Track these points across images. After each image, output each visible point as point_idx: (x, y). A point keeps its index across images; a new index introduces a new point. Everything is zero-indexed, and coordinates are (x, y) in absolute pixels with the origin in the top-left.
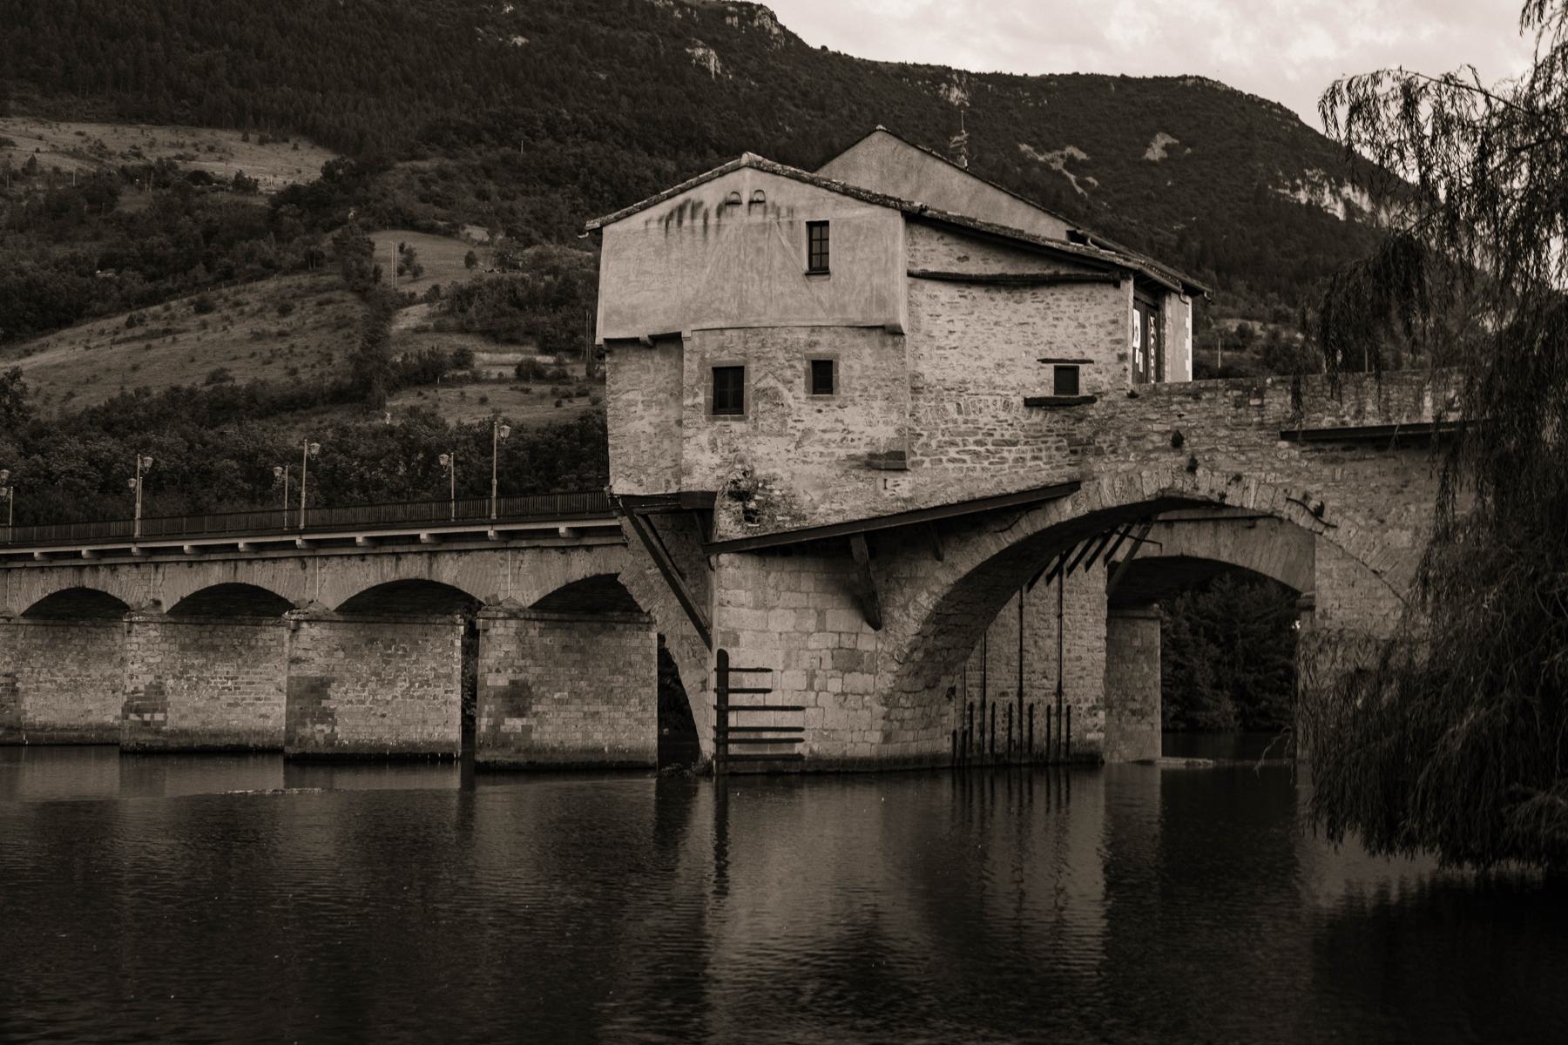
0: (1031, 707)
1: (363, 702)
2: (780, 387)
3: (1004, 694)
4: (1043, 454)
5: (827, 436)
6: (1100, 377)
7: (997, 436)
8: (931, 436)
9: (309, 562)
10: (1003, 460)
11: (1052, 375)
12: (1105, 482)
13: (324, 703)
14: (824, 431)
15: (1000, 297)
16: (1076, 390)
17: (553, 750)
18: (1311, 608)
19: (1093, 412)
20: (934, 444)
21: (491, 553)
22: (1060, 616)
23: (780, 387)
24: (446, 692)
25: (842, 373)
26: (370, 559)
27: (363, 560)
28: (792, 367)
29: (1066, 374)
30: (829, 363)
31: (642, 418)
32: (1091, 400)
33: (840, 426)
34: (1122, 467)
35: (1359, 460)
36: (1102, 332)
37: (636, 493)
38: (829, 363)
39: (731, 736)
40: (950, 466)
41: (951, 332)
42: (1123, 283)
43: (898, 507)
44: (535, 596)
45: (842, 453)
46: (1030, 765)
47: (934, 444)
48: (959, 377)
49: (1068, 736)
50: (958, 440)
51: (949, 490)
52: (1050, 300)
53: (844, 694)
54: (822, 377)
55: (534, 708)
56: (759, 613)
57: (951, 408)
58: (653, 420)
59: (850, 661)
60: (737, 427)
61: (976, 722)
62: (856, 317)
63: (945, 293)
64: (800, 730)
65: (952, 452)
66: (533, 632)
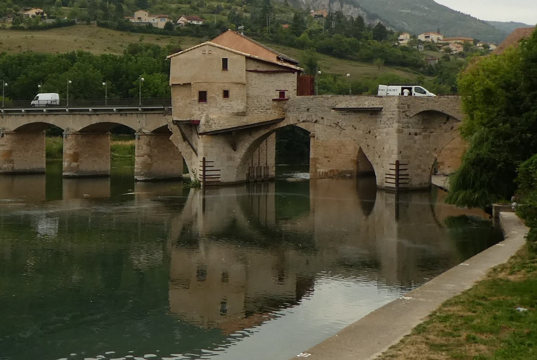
0: (261, 167)
1: (21, 157)
2: (216, 96)
3: (256, 164)
4: (277, 111)
5: (227, 108)
6: (289, 94)
7: (266, 108)
8: (251, 108)
9: (4, 116)
10: (267, 113)
11: (279, 93)
12: (291, 118)
13: (11, 158)
14: (226, 107)
15: (267, 76)
16: (284, 97)
17: (85, 171)
18: (314, 137)
19: (288, 102)
20: (252, 109)
21: (66, 115)
22: (266, 144)
23: (216, 96)
24: (42, 153)
25: (230, 94)
26: (25, 116)
27: (23, 116)
28: (219, 91)
29: (282, 94)
30: (228, 91)
31: (180, 102)
32: (288, 99)
33: (230, 106)
34: (295, 115)
35: (351, 114)
36: (290, 84)
37: (179, 120)
38: (228, 91)
39: (206, 177)
40: (255, 115)
41: (255, 84)
42: (295, 73)
43: (243, 124)
44: (80, 128)
45: (231, 112)
46: (261, 181)
47: (252, 109)
48: (257, 94)
49: (268, 174)
50: (257, 109)
51: (255, 120)
52: (278, 76)
53: (228, 166)
54: (226, 94)
55: (80, 159)
56: (211, 148)
57: (256, 101)
58: (183, 103)
59: (230, 159)
60: (205, 105)
61: (251, 171)
62: (234, 80)
63: (254, 75)
64: (220, 175)
65: (256, 111)
66: (79, 138)
